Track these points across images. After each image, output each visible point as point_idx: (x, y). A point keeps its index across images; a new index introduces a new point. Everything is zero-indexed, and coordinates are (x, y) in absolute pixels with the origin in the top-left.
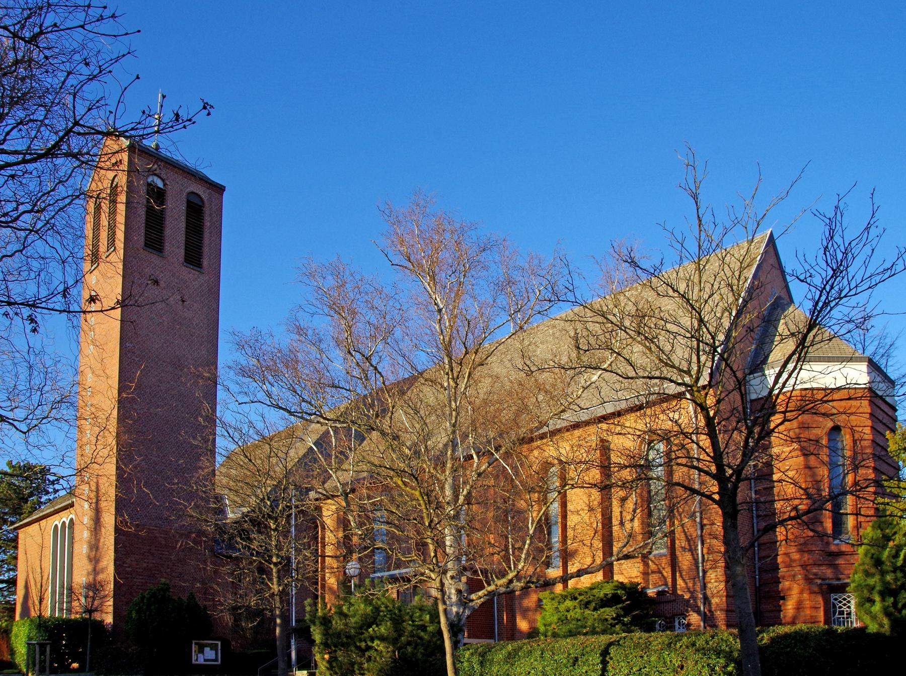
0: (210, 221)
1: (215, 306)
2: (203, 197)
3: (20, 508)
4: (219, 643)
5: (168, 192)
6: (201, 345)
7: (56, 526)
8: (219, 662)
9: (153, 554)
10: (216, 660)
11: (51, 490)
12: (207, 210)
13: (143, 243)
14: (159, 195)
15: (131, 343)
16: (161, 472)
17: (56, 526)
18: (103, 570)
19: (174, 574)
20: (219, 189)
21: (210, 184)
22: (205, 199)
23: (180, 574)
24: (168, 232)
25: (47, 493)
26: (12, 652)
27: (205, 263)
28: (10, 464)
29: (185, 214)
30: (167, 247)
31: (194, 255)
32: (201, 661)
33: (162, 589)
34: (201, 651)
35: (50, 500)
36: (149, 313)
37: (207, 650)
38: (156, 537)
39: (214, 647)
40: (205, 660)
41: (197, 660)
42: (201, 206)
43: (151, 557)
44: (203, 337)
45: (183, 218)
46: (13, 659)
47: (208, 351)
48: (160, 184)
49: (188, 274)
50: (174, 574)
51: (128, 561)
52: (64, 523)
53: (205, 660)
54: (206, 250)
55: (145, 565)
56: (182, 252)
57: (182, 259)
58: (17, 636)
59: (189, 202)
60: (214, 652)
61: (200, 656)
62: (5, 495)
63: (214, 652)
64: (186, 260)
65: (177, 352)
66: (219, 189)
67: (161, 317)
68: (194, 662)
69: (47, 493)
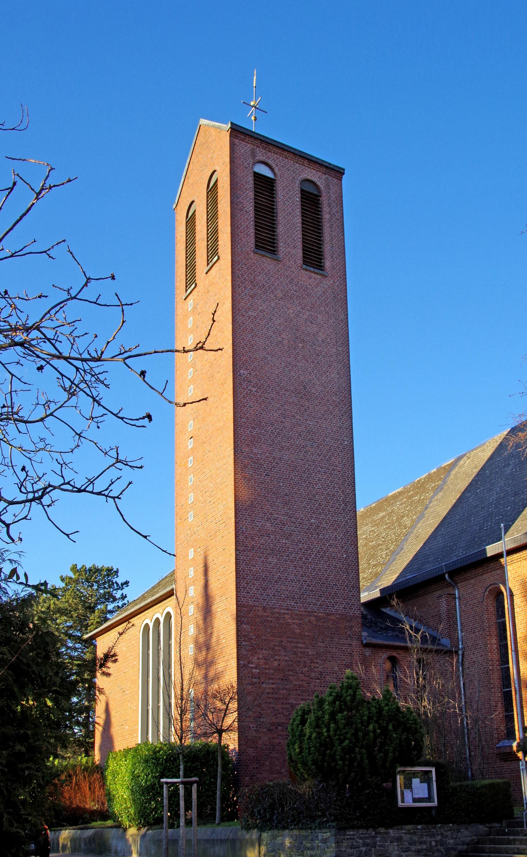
0: (329, 213)
1: (342, 317)
2: (319, 183)
3: (86, 618)
4: (433, 770)
5: (278, 182)
6: (330, 366)
7: (147, 625)
8: (435, 803)
9: (285, 648)
10: (430, 799)
11: (118, 596)
12: (324, 200)
13: (253, 246)
14: (265, 186)
15: (247, 369)
16: (290, 535)
17: (147, 625)
18: (217, 677)
19: (313, 674)
20: (344, 170)
21: (326, 167)
22: (322, 187)
23: (321, 674)
24: (280, 229)
25: (115, 599)
26: (109, 797)
27: (327, 264)
28: (74, 568)
29: (299, 207)
30: (282, 248)
31: (313, 256)
32: (409, 802)
33: (349, 687)
34: (408, 785)
35: (119, 607)
36: (265, 331)
37: (416, 781)
38: (288, 624)
39: (425, 777)
40: (415, 800)
41: (403, 801)
42: (317, 196)
43: (283, 653)
44: (331, 356)
45: (298, 212)
46: (110, 806)
47: (338, 373)
48: (270, 175)
49: (308, 278)
50: (313, 674)
51: (255, 660)
52: (157, 620)
53: (415, 800)
54: (327, 248)
55: (276, 663)
56: (299, 253)
57: (300, 261)
58: (115, 774)
59: (302, 191)
60: (425, 785)
61: (407, 793)
62: (70, 605)
63: (425, 785)
64: (305, 262)
65: (302, 378)
66: (338, 172)
67: (280, 334)
68: (400, 804)
69: (115, 599)
